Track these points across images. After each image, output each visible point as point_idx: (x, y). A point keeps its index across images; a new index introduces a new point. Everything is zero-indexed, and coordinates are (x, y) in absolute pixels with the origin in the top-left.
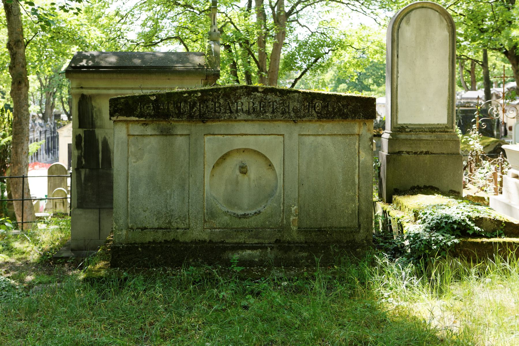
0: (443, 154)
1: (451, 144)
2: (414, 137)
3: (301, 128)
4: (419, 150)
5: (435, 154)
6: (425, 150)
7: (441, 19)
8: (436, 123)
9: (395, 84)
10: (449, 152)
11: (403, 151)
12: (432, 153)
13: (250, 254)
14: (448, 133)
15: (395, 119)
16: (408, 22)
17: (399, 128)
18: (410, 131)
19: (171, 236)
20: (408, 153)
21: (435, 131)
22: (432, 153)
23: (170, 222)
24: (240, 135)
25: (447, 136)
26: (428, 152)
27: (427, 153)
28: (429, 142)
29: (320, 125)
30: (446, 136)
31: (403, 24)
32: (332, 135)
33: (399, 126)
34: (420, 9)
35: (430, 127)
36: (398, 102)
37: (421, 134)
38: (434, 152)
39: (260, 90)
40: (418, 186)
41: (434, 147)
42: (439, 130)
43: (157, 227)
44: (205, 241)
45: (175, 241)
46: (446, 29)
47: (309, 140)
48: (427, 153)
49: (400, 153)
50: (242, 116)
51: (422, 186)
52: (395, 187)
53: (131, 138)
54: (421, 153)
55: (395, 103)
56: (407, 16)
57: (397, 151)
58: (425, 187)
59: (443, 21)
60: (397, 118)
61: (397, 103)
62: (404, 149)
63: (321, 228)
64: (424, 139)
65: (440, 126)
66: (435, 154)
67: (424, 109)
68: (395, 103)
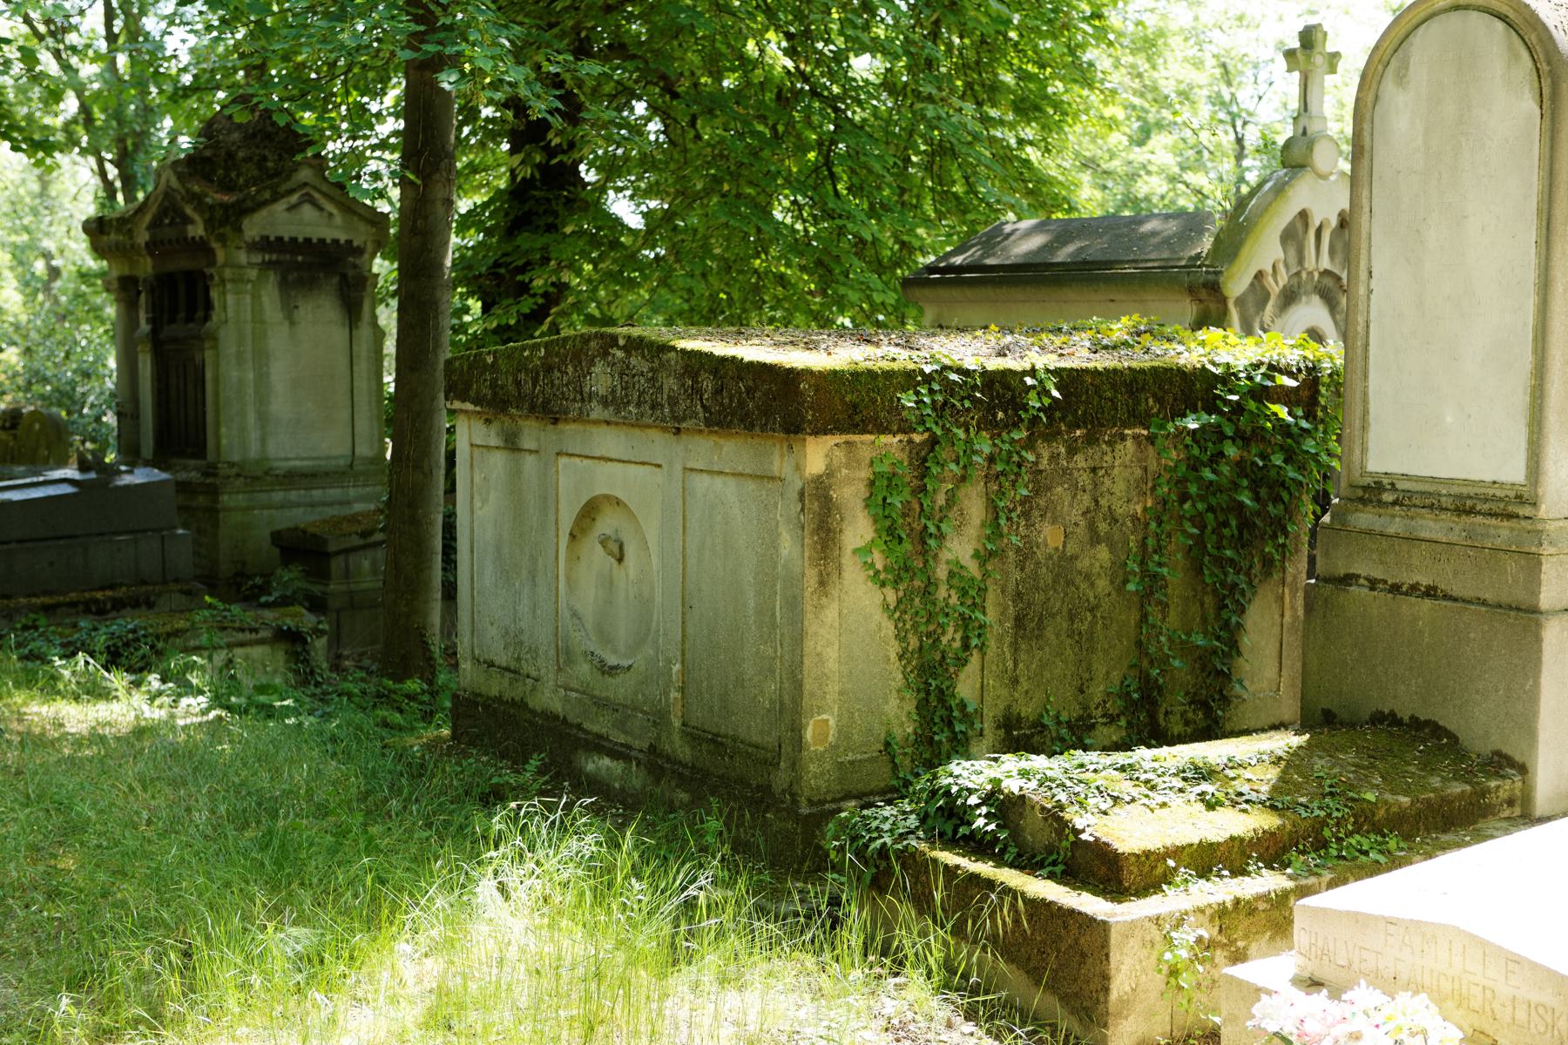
0: (1484, 603)
1: (1511, 566)
2: (1395, 526)
3: (687, 450)
4: (1408, 579)
5: (1456, 600)
6: (1425, 581)
7: (1511, 48)
8: (1488, 478)
9: (1361, 319)
10: (1505, 599)
11: (1359, 576)
12: (1446, 597)
13: (608, 768)
14: (1513, 523)
15: (1357, 452)
16: (1401, 79)
17: (1366, 488)
18: (1395, 503)
19: (516, 693)
20: (1373, 584)
21: (1471, 511)
22: (1446, 597)
23: (519, 659)
24: (600, 458)
25: (1505, 533)
26: (1435, 588)
27: (1430, 592)
28: (1439, 548)
29: (716, 444)
30: (1503, 531)
31: (1389, 86)
32: (762, 477)
33: (1368, 480)
34: (1443, 16)
35: (1465, 491)
36: (1371, 389)
37: (1423, 518)
38: (1456, 591)
39: (621, 342)
40: (1392, 714)
41: (1456, 573)
42: (1486, 507)
43: (504, 664)
44: (556, 717)
45: (521, 705)
46: (1527, 89)
47: (701, 483)
48: (1430, 592)
49: (1349, 579)
50: (597, 412)
51: (1406, 719)
52: (1325, 704)
53: (476, 452)
54: (1414, 588)
55: (1358, 395)
56: (1400, 51)
57: (1342, 572)
58: (1385, 720)
59: (1517, 57)
60: (1364, 450)
61: (1365, 394)
62: (1362, 568)
63: (718, 735)
64: (1423, 535)
65: (1499, 493)
66: (1456, 600)
67: (1449, 419)
68: (1358, 395)
